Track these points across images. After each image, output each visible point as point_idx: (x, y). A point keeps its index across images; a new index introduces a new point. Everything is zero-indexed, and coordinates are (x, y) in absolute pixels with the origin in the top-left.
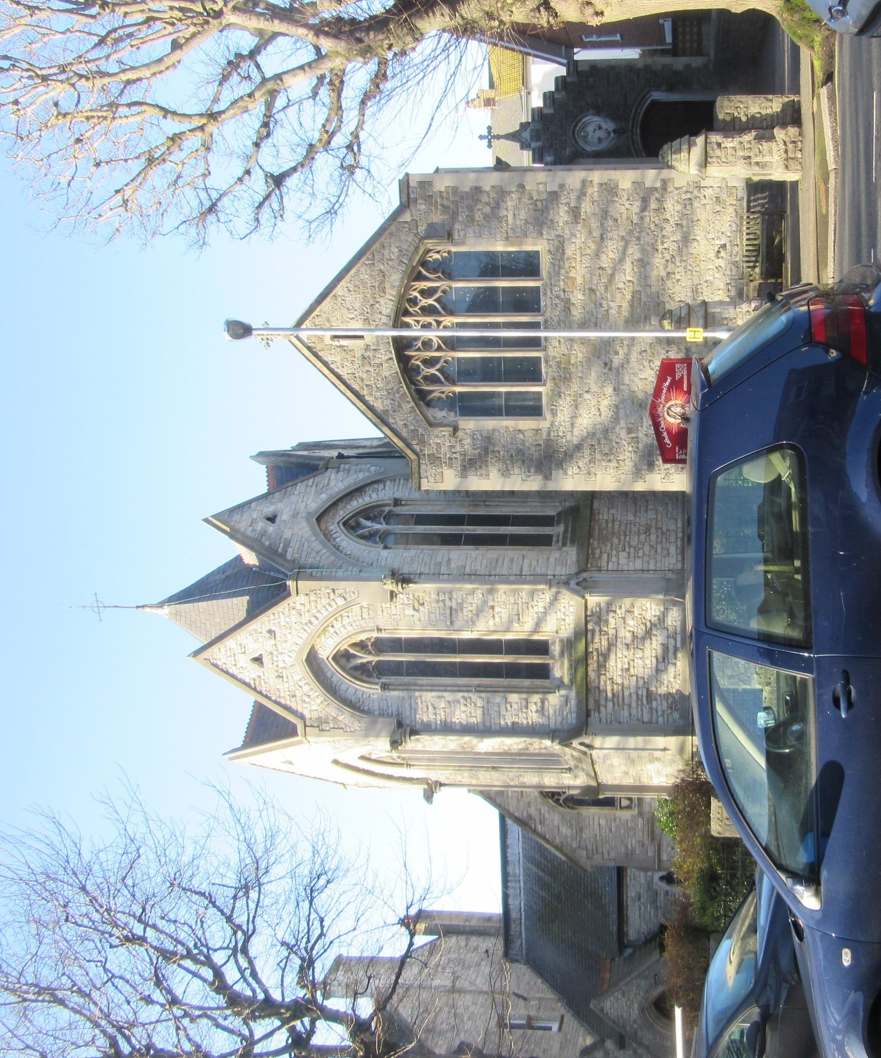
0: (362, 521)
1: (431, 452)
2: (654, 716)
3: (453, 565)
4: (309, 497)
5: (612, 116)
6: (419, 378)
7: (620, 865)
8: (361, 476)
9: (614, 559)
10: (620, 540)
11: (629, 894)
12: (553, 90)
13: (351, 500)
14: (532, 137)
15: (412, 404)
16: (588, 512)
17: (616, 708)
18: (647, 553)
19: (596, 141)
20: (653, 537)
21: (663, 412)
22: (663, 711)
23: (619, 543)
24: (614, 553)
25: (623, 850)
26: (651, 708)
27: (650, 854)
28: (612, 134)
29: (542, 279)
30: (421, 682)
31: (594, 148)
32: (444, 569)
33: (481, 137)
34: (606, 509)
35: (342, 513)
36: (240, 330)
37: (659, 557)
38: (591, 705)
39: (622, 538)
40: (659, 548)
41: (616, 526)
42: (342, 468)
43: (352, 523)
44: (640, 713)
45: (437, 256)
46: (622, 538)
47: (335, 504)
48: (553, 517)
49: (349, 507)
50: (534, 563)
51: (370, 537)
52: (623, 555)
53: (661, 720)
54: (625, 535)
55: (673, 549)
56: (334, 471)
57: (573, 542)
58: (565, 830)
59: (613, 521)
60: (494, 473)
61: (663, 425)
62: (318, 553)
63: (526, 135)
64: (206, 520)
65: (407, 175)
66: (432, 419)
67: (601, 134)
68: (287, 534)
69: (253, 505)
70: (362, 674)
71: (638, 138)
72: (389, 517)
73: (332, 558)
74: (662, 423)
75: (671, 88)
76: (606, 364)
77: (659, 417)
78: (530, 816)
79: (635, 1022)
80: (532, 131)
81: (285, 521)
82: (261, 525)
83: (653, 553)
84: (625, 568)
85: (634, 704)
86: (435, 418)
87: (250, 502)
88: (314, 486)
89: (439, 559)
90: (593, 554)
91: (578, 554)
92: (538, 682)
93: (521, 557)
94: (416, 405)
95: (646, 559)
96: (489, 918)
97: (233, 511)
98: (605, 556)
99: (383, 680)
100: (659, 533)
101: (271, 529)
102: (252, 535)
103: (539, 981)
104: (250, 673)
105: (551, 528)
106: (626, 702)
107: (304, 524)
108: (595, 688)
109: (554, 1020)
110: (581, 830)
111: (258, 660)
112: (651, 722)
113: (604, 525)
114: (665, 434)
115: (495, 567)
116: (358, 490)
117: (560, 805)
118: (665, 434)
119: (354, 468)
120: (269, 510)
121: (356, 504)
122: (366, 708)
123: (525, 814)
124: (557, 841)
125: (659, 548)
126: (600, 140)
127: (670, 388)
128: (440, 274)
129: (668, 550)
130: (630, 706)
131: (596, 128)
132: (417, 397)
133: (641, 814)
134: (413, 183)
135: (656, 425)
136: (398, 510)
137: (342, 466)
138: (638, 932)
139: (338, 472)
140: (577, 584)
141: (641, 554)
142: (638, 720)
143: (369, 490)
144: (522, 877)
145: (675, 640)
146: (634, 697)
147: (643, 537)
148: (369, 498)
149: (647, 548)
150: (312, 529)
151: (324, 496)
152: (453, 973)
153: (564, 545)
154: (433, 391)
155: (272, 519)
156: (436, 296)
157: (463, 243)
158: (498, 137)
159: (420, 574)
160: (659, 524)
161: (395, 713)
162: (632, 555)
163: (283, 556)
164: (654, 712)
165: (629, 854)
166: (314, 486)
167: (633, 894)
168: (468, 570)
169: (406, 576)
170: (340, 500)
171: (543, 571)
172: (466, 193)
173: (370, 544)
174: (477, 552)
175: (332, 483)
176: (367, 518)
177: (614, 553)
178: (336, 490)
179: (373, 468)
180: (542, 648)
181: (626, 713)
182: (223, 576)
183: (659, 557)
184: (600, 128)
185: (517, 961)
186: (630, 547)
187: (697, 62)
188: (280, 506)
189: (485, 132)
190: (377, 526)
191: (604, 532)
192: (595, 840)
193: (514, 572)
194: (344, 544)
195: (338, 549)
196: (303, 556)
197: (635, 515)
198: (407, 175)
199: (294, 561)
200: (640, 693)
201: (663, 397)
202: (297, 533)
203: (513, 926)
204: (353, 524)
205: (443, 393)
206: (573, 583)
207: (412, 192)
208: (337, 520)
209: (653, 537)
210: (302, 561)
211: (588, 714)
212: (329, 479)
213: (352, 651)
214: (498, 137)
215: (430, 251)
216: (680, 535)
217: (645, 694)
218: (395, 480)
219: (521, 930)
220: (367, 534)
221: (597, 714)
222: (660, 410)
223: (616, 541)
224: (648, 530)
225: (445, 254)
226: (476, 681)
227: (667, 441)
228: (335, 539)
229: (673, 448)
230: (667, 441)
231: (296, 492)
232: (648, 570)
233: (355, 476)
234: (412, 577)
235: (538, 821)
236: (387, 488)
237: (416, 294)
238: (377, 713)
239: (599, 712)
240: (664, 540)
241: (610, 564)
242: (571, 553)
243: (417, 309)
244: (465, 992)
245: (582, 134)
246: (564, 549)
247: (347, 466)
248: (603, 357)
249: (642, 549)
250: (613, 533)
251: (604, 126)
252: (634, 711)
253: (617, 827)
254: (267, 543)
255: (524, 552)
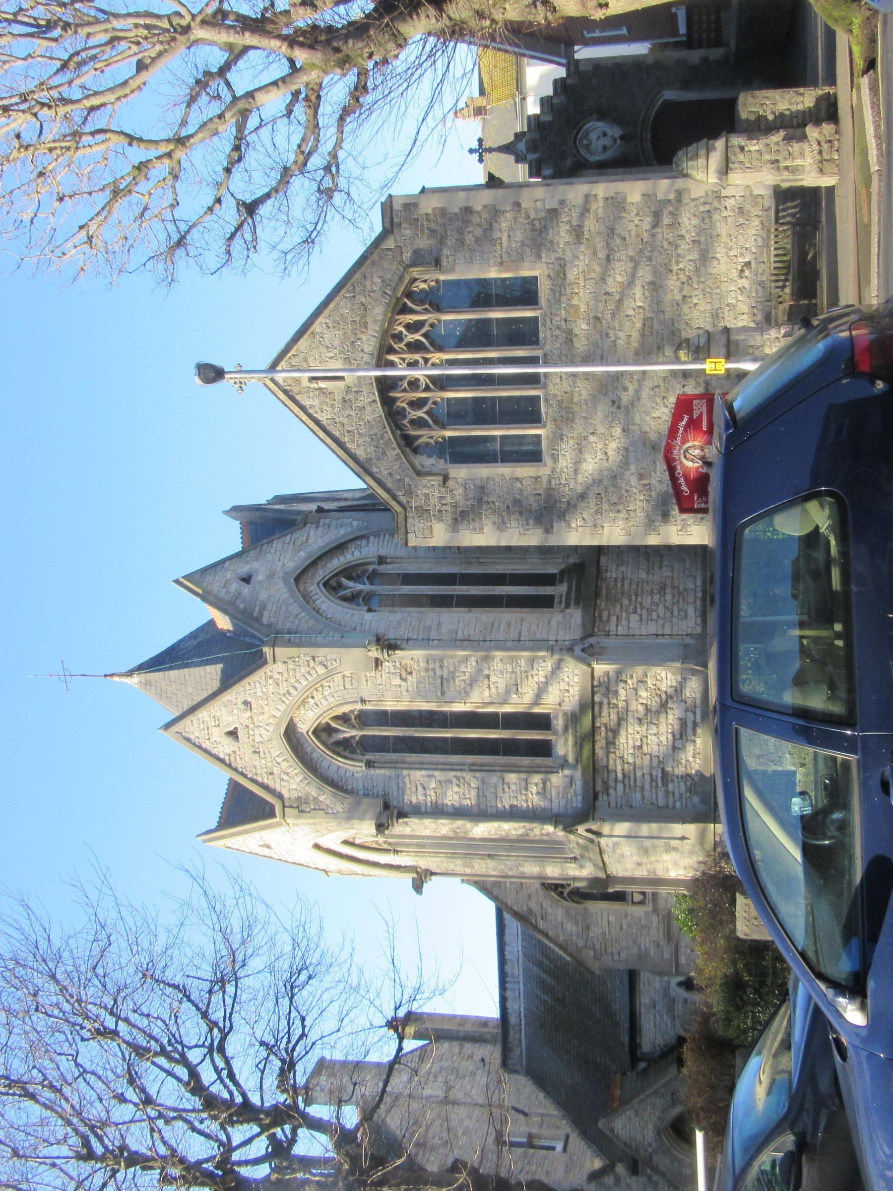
0: (344, 581)
1: (418, 504)
2: (671, 799)
3: (444, 629)
4: (286, 555)
5: (617, 121)
6: (405, 422)
7: (632, 967)
8: (342, 532)
9: (624, 622)
10: (630, 600)
11: (643, 1001)
12: (551, 93)
13: (332, 558)
14: (528, 149)
15: (398, 451)
16: (594, 569)
17: (627, 790)
18: (661, 615)
19: (600, 150)
20: (669, 597)
21: (679, 455)
22: (681, 795)
23: (630, 604)
24: (624, 615)
25: (635, 950)
26: (667, 792)
27: (666, 956)
28: (619, 141)
29: (541, 309)
30: (409, 759)
31: (598, 158)
32: (434, 635)
33: (471, 151)
34: (614, 566)
35: (324, 571)
36: (212, 374)
37: (675, 620)
38: (599, 787)
39: (633, 598)
40: (675, 609)
41: (626, 585)
42: (321, 523)
43: (333, 583)
44: (654, 796)
45: (423, 286)
46: (633, 598)
47: (314, 563)
48: (555, 574)
49: (329, 565)
50: (534, 627)
51: (351, 599)
52: (634, 618)
53: (678, 804)
54: (637, 596)
55: (691, 611)
56: (314, 526)
57: (577, 603)
58: (570, 928)
59: (623, 579)
60: (488, 528)
61: (679, 470)
62: (296, 617)
63: (522, 146)
64: (177, 582)
65: (390, 196)
66: (420, 467)
67: (606, 141)
68: (263, 596)
69: (227, 564)
70: (345, 750)
71: (648, 145)
72: (373, 577)
73: (312, 622)
74: (679, 467)
75: (685, 85)
76: (613, 402)
77: (675, 460)
78: (530, 911)
79: (650, 1145)
80: (527, 141)
81: (260, 582)
82: (234, 586)
83: (668, 614)
84: (637, 632)
85: (647, 787)
86: (423, 466)
87: (223, 561)
88: (292, 545)
89: (428, 623)
90: (601, 616)
91: (583, 619)
92: (539, 760)
93: (519, 621)
94: (403, 452)
95: (661, 622)
96: (485, 1023)
97: (204, 571)
98: (614, 619)
99: (367, 757)
100: (676, 593)
101: (246, 590)
102: (226, 598)
103: (541, 1095)
104: (225, 747)
105: (552, 588)
106: (639, 783)
107: (281, 584)
108: (604, 767)
109: (558, 1139)
110: (588, 927)
111: (233, 734)
112: (667, 807)
113: (612, 584)
114: (682, 480)
115: (491, 632)
116: (340, 548)
117: (565, 899)
118: (682, 480)
119: (334, 522)
120: (244, 569)
121: (337, 563)
122: (349, 788)
123: (525, 908)
124: (561, 939)
125: (675, 609)
126: (605, 148)
127: (686, 427)
128: (427, 306)
129: (686, 612)
130: (643, 788)
131: (600, 136)
132: (403, 443)
133: (655, 910)
134: (397, 206)
135: (671, 470)
136: (382, 568)
137: (322, 521)
138: (654, 1044)
139: (317, 527)
140: (583, 650)
141: (654, 616)
142: (652, 804)
143: (351, 547)
144: (521, 978)
145: (695, 713)
146: (647, 777)
147: (656, 597)
148: (351, 556)
149: (661, 610)
150: (290, 590)
151: (302, 554)
152: (446, 1082)
153: (568, 606)
154: (419, 437)
155: (247, 580)
156: (423, 331)
157: (452, 270)
158: (490, 150)
159: (408, 640)
160: (676, 583)
161: (381, 793)
162: (644, 618)
163: (258, 620)
164: (670, 795)
165: (643, 956)
166: (292, 545)
167: (647, 1001)
168: (460, 636)
169: (392, 642)
170: (320, 557)
171: (544, 636)
172: (456, 214)
173: (352, 606)
174: (470, 615)
175: (311, 541)
176: (350, 578)
177: (624, 615)
178: (316, 546)
179: (355, 523)
180: (542, 722)
181: (638, 796)
182: (195, 643)
183: (675, 620)
184: (605, 134)
185: (516, 1072)
186: (642, 608)
187: (716, 54)
188: (256, 565)
189: (475, 145)
190: (360, 587)
191: (613, 592)
192: (604, 939)
193: (512, 637)
194: (324, 607)
195: (318, 612)
196: (281, 621)
197: (648, 573)
198: (390, 196)
199: (270, 626)
200: (654, 773)
201: (679, 439)
202: (274, 595)
203: (512, 1032)
204: (334, 584)
205: (431, 438)
206: (578, 650)
207: (396, 215)
208: (317, 581)
209: (669, 597)
210: (280, 626)
211: (595, 797)
212: (308, 536)
213: (333, 725)
214: (490, 150)
215: (416, 280)
216: (699, 595)
217: (660, 775)
218: (379, 536)
219: (521, 1038)
220: (349, 595)
221: (605, 797)
222: (675, 452)
223: (626, 601)
224: (662, 589)
225: (433, 284)
226: (469, 759)
227: (684, 488)
228: (314, 601)
229: (691, 497)
230: (684, 488)
231: (273, 550)
232: (663, 635)
233: (336, 532)
234: (399, 642)
235: (539, 916)
236: (371, 544)
237: (401, 328)
238: (361, 793)
239: (608, 795)
240: (681, 601)
241: (620, 628)
242: (576, 616)
243: (402, 345)
244: (458, 1104)
245: (585, 142)
246: (567, 611)
247: (327, 521)
248: (610, 394)
249: (656, 610)
250: (622, 593)
251: (610, 132)
252: (647, 795)
253: (629, 924)
254: (242, 606)
255: (523, 615)
